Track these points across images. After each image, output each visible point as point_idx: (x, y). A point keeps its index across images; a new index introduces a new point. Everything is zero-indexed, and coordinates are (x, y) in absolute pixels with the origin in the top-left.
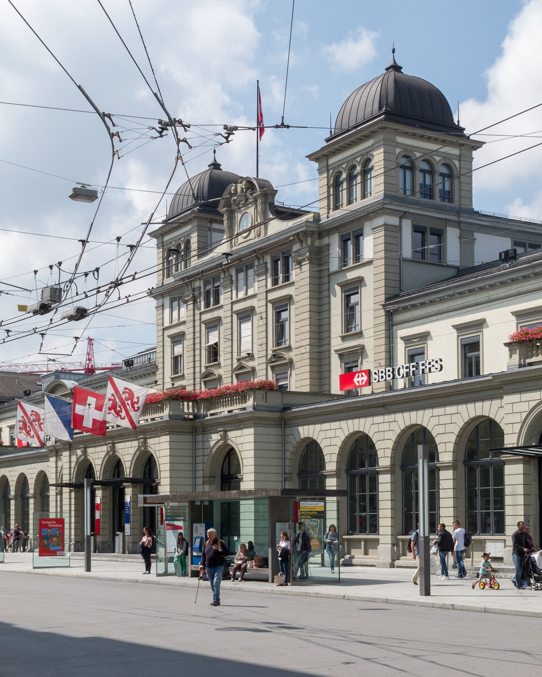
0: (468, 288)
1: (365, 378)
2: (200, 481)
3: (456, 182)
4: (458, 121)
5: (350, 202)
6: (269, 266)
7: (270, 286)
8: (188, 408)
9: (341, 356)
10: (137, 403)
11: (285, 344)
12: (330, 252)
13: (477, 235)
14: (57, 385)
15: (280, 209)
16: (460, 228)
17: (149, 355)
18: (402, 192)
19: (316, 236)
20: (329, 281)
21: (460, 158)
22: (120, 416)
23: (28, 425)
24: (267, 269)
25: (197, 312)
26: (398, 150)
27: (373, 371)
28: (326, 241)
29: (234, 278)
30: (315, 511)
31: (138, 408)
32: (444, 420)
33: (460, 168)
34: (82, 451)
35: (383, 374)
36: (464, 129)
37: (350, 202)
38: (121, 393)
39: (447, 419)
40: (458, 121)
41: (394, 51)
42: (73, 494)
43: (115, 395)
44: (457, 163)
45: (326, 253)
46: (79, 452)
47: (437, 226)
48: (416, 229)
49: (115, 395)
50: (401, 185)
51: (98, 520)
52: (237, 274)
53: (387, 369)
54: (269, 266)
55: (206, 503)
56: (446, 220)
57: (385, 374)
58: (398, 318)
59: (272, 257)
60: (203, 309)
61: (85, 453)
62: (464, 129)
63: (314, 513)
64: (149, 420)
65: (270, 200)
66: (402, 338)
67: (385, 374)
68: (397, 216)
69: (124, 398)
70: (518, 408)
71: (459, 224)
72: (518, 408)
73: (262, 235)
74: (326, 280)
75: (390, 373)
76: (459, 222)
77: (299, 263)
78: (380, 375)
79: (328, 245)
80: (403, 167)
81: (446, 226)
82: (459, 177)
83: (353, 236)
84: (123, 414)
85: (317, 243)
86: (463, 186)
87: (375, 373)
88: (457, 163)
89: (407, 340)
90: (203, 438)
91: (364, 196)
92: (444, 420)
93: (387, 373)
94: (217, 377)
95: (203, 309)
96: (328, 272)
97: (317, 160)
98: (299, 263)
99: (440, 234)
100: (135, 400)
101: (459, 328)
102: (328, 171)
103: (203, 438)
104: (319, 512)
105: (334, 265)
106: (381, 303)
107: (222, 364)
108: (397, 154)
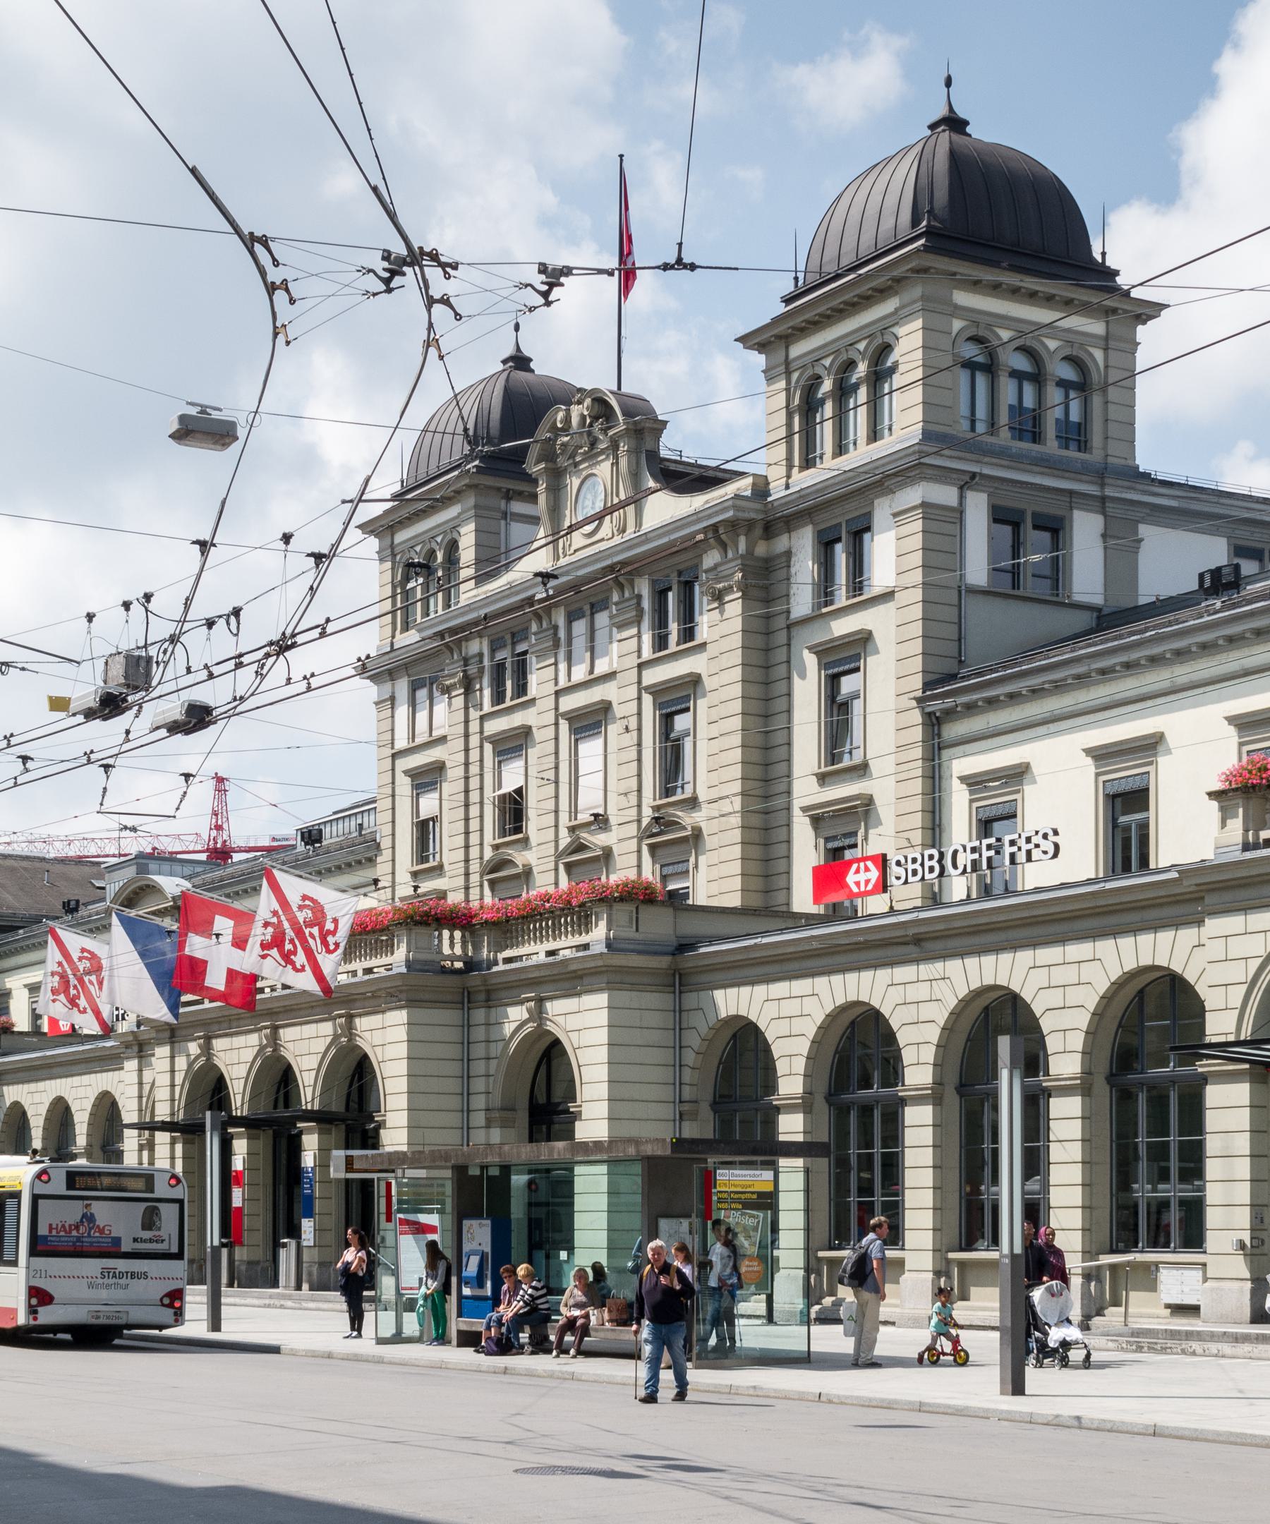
0: (1124, 658)
1: (874, 874)
2: (479, 1119)
3: (1097, 400)
4: (1104, 254)
5: (840, 450)
6: (646, 604)
7: (647, 653)
8: (452, 945)
9: (816, 821)
10: (334, 933)
11: (683, 793)
12: (793, 570)
13: (1144, 530)
14: (141, 888)
15: (673, 467)
16: (1104, 514)
17: (359, 816)
18: (965, 425)
19: (758, 531)
20: (789, 639)
21: (1106, 343)
22: (293, 964)
23: (287, 938)
24: (640, 612)
25: (474, 714)
26: (957, 325)
27: (893, 858)
28: (781, 543)
29: (562, 634)
30: (753, 1193)
31: (337, 945)
32: (1060, 975)
33: (1106, 367)
34: (200, 1046)
35: (917, 866)
36: (1116, 273)
37: (840, 450)
38: (295, 909)
39: (1069, 975)
40: (1104, 254)
41: (948, 83)
42: (179, 1148)
43: (281, 912)
44: (1098, 355)
45: (781, 574)
46: (194, 1048)
47: (1052, 508)
48: (999, 516)
49: (281, 912)
50: (964, 409)
51: (239, 1210)
52: (570, 621)
53: (927, 853)
54: (646, 604)
55: (495, 1172)
56: (1071, 493)
57: (922, 865)
58: (953, 730)
59: (653, 583)
60: (487, 707)
61: (207, 1049)
62: (1116, 273)
63: (749, 1196)
64: (360, 973)
65: (649, 445)
66: (963, 779)
67: (922, 865)
68: (953, 484)
69: (301, 921)
70: (1240, 947)
71: (1104, 503)
72: (1240, 947)
73: (631, 528)
74: (781, 637)
75: (934, 863)
76: (1103, 500)
77: (718, 597)
78: (911, 867)
79: (788, 554)
80: (970, 365)
81: (1071, 509)
82: (1104, 389)
83: (848, 532)
84: (300, 958)
85: (761, 549)
86: (1113, 412)
87: (898, 863)
88: (1098, 355)
89: (975, 782)
90: (488, 1016)
91: (874, 436)
92: (1060, 975)
93: (927, 864)
94: (520, 870)
95: (487, 707)
96: (788, 618)
97: (762, 347)
98: (718, 597)
99: (1056, 529)
100: (329, 926)
101: (1101, 755)
102: (788, 373)
103: (488, 1016)
104: (761, 1195)
105: (802, 601)
106: (912, 695)
107: (534, 840)
108: (954, 334)
